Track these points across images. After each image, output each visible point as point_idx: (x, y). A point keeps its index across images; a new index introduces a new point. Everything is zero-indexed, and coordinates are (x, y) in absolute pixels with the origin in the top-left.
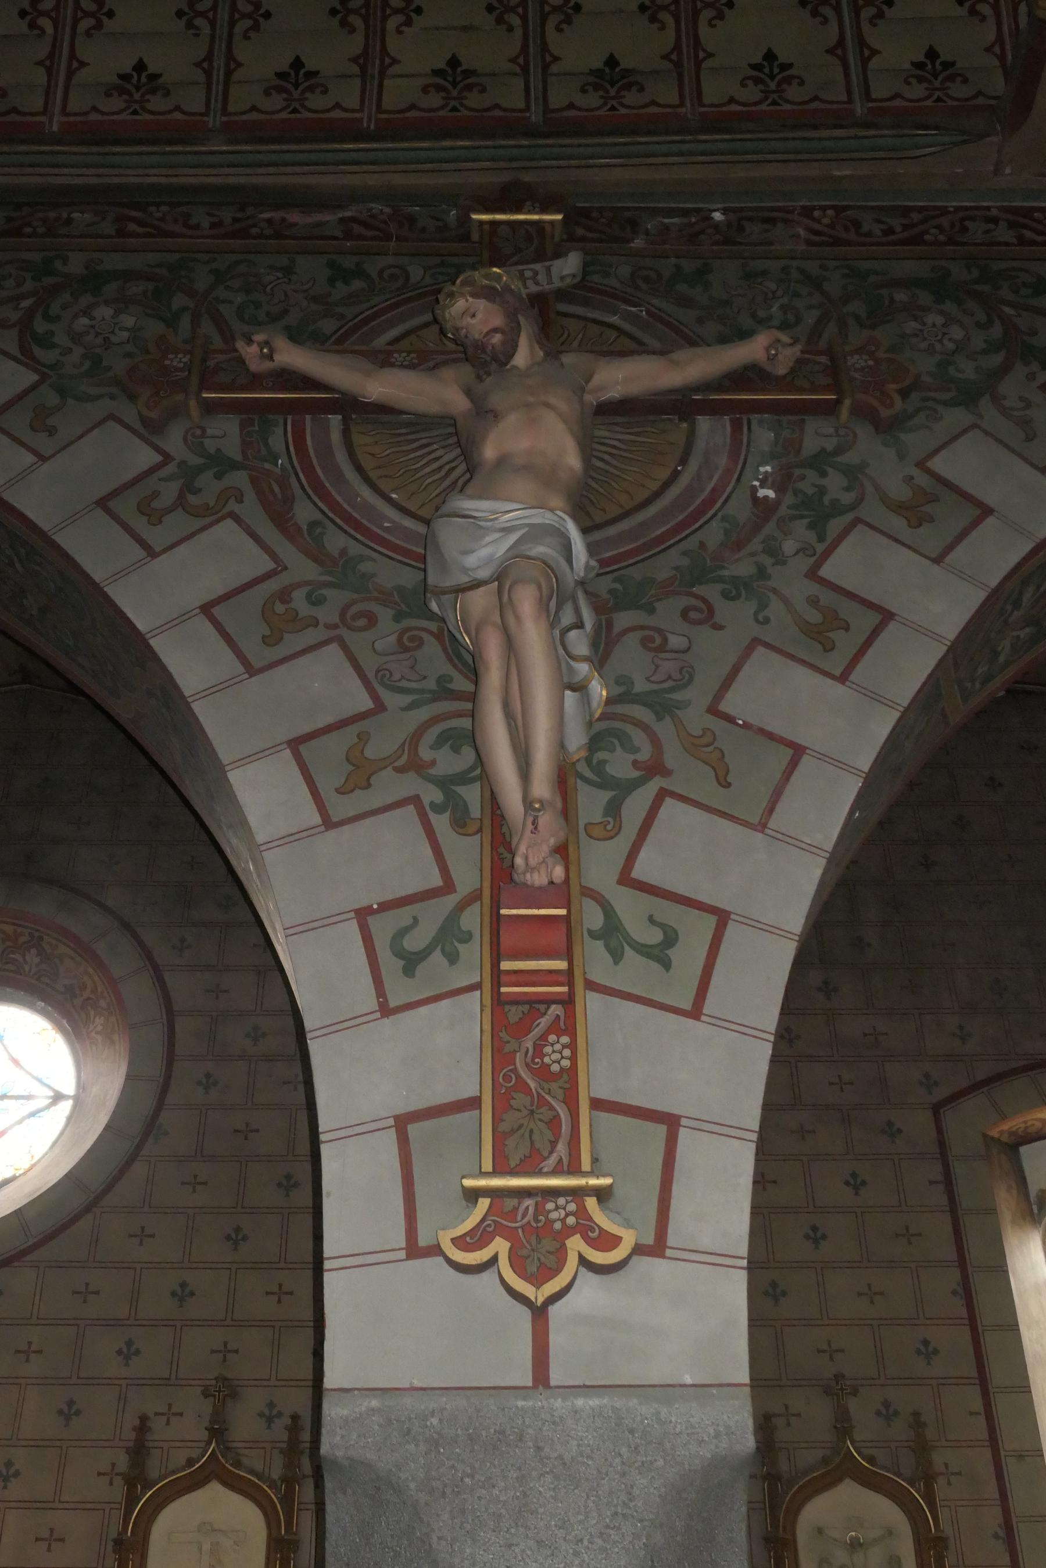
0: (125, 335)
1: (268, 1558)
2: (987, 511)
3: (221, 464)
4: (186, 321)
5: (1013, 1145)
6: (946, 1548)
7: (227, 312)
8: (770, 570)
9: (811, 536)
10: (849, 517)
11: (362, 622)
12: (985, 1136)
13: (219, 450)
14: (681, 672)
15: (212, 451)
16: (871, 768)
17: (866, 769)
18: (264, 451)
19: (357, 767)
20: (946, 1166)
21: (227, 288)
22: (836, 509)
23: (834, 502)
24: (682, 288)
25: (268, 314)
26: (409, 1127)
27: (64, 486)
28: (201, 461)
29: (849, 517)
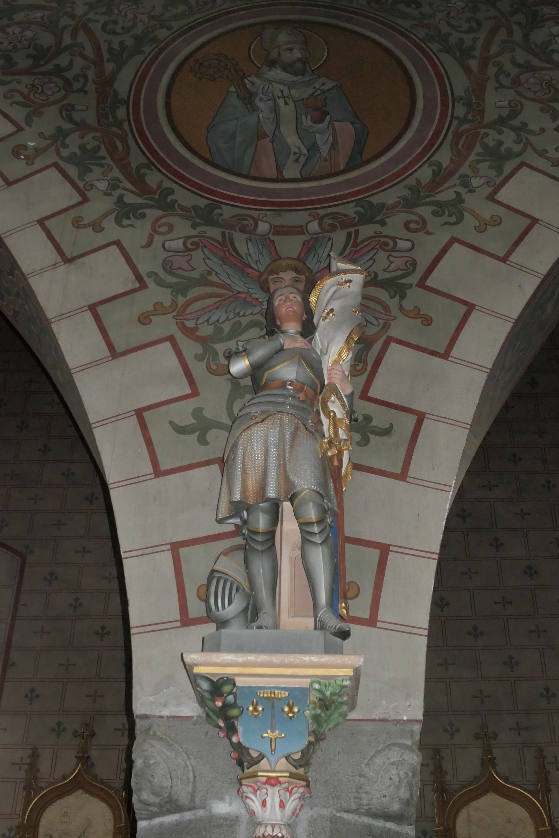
7: (97, 28)
8: (464, 196)
9: (493, 173)
10: (518, 160)
11: (164, 229)
14: (406, 265)
15: (78, 120)
18: (111, 120)
21: (96, 13)
22: (510, 155)
23: (509, 150)
25: (123, 28)
26: (443, 352)
29: (518, 160)
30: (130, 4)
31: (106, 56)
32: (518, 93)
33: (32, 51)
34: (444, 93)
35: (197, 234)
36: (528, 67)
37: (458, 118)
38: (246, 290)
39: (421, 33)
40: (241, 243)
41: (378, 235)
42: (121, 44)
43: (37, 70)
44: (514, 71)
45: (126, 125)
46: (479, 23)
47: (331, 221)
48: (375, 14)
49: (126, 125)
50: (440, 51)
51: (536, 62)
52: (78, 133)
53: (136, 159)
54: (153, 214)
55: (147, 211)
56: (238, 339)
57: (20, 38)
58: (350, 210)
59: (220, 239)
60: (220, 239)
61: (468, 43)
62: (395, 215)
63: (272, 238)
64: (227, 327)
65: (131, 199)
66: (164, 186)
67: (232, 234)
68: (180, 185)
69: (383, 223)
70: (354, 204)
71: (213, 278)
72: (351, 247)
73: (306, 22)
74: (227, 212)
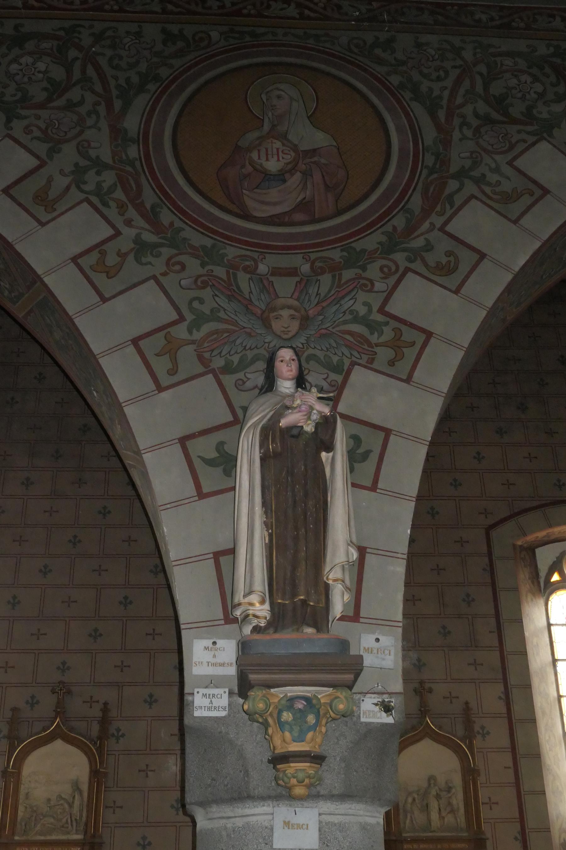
0: (41, 75)
1: (90, 780)
2: (546, 192)
3: (100, 166)
4: (77, 65)
5: (531, 550)
6: (479, 775)
7: (103, 62)
11: (178, 267)
12: (514, 546)
13: (98, 157)
16: (448, 391)
17: (445, 391)
19: (169, 342)
20: (491, 561)
24: (378, 51)
27: (52, 251)
28: (87, 163)
30: (134, 38)
31: (115, 92)
32: (477, 143)
33: (45, 84)
34: (416, 144)
35: (205, 273)
36: (487, 120)
37: (427, 167)
38: (250, 326)
39: (395, 80)
40: (243, 279)
41: (360, 277)
42: (128, 80)
43: (52, 105)
44: (475, 123)
45: (137, 164)
46: (447, 73)
47: (320, 264)
48: (352, 57)
49: (137, 164)
50: (411, 99)
51: (495, 116)
52: (95, 170)
53: (149, 197)
54: (166, 252)
55: (164, 250)
56: (245, 371)
57: (33, 69)
58: (336, 255)
59: (224, 277)
60: (224, 277)
61: (436, 93)
62: (374, 261)
63: (272, 279)
64: (236, 359)
65: (149, 237)
66: (176, 225)
67: (342, 375)
68: (190, 226)
69: (364, 268)
70: (339, 249)
71: (222, 314)
72: (337, 287)
73: (302, 66)
74: (232, 252)
